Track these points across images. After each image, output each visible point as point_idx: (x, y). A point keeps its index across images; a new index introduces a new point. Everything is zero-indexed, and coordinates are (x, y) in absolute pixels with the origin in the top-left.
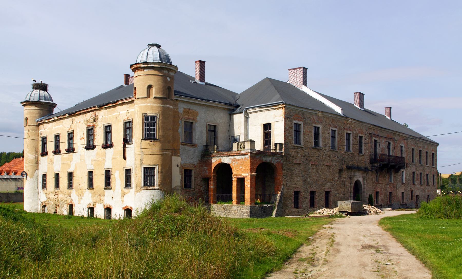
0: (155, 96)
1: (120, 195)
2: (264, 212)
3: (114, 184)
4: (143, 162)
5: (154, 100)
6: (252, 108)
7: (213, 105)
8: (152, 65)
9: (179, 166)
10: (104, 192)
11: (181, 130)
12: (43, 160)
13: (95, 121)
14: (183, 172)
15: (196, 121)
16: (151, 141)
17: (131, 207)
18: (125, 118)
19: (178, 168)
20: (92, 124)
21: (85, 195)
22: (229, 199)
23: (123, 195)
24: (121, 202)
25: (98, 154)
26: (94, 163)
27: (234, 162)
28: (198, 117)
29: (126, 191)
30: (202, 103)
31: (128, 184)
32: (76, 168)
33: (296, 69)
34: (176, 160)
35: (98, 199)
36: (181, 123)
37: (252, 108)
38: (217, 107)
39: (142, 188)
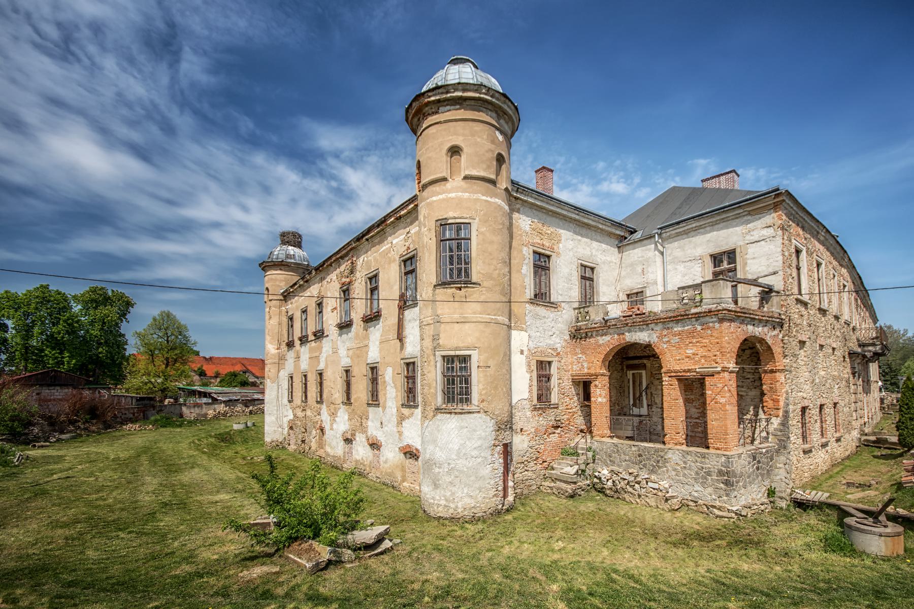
0: (467, 173)
1: (395, 420)
2: (758, 468)
3: (385, 394)
4: (441, 341)
5: (463, 184)
6: (678, 223)
7: (591, 222)
8: (459, 94)
9: (526, 353)
10: (367, 412)
11: (526, 271)
12: (291, 355)
13: (352, 272)
14: (534, 368)
15: (558, 254)
16: (460, 289)
17: (417, 450)
18: (402, 250)
19: (523, 357)
20: (348, 280)
21: (339, 414)
22: (650, 431)
23: (402, 419)
24: (397, 435)
25: (357, 336)
26: (351, 352)
27: (665, 339)
28: (561, 245)
29: (406, 411)
30: (570, 215)
31: (410, 396)
32: (327, 365)
33: (718, 176)
34: (519, 339)
35: (358, 424)
36: (527, 252)
37: (678, 223)
38: (596, 229)
39: (438, 410)
